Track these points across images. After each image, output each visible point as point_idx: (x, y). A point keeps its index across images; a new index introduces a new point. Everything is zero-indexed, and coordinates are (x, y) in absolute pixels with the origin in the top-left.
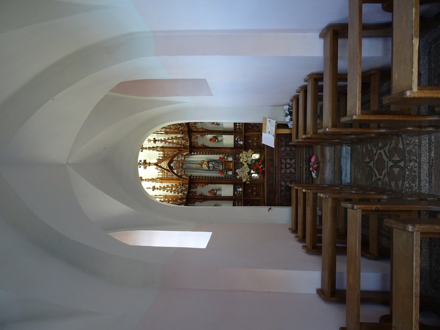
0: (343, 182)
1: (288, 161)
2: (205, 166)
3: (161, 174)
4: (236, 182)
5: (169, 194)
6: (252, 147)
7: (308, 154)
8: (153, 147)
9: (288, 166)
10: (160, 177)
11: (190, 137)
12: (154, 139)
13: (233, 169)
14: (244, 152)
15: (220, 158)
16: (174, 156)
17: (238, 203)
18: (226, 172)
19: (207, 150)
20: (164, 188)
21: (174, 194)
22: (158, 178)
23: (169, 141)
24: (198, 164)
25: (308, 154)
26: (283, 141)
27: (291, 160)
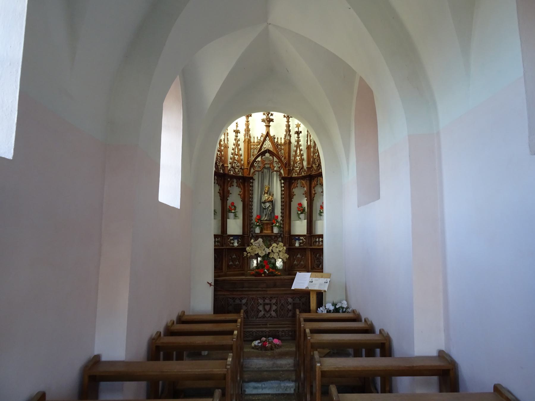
0: (246, 385)
1: (274, 307)
2: (266, 197)
3: (256, 141)
4: (245, 238)
5: (230, 151)
6: (292, 259)
7: (283, 333)
8: (290, 131)
9: (267, 308)
10: (252, 140)
11: (303, 178)
12: (301, 132)
13: (263, 234)
14: (285, 248)
15: (277, 217)
16: (278, 158)
17: (218, 242)
18: (259, 226)
19: (287, 200)
20: (237, 145)
21: (229, 158)
22: (250, 137)
23: (298, 151)
24: (269, 188)
25: (283, 333)
26: (300, 300)
27: (276, 311)
